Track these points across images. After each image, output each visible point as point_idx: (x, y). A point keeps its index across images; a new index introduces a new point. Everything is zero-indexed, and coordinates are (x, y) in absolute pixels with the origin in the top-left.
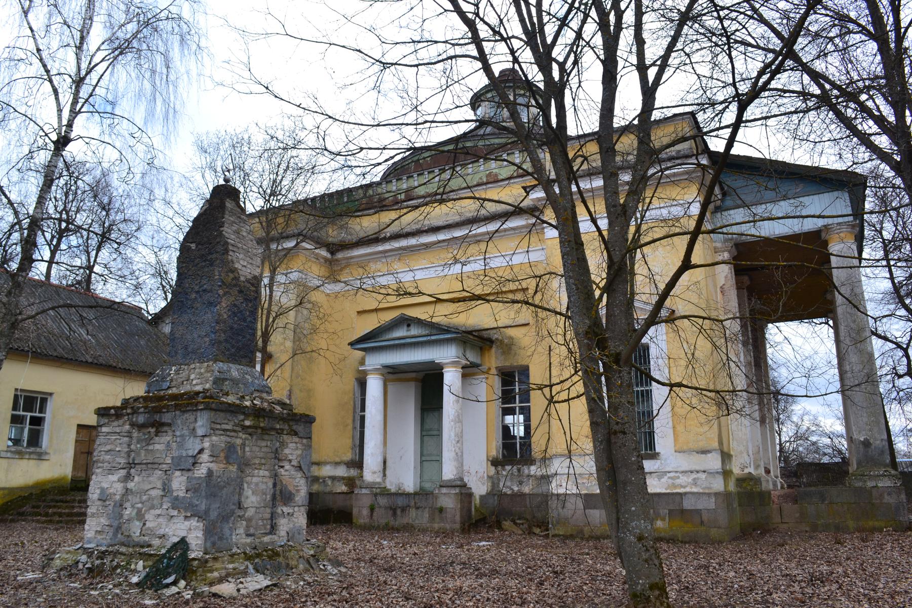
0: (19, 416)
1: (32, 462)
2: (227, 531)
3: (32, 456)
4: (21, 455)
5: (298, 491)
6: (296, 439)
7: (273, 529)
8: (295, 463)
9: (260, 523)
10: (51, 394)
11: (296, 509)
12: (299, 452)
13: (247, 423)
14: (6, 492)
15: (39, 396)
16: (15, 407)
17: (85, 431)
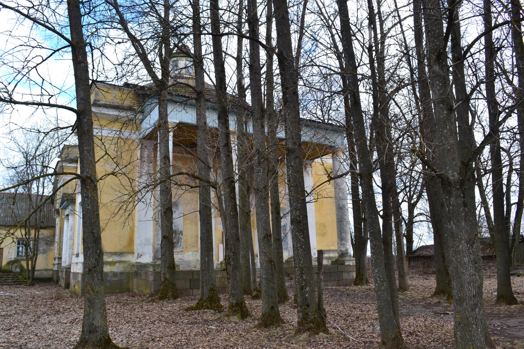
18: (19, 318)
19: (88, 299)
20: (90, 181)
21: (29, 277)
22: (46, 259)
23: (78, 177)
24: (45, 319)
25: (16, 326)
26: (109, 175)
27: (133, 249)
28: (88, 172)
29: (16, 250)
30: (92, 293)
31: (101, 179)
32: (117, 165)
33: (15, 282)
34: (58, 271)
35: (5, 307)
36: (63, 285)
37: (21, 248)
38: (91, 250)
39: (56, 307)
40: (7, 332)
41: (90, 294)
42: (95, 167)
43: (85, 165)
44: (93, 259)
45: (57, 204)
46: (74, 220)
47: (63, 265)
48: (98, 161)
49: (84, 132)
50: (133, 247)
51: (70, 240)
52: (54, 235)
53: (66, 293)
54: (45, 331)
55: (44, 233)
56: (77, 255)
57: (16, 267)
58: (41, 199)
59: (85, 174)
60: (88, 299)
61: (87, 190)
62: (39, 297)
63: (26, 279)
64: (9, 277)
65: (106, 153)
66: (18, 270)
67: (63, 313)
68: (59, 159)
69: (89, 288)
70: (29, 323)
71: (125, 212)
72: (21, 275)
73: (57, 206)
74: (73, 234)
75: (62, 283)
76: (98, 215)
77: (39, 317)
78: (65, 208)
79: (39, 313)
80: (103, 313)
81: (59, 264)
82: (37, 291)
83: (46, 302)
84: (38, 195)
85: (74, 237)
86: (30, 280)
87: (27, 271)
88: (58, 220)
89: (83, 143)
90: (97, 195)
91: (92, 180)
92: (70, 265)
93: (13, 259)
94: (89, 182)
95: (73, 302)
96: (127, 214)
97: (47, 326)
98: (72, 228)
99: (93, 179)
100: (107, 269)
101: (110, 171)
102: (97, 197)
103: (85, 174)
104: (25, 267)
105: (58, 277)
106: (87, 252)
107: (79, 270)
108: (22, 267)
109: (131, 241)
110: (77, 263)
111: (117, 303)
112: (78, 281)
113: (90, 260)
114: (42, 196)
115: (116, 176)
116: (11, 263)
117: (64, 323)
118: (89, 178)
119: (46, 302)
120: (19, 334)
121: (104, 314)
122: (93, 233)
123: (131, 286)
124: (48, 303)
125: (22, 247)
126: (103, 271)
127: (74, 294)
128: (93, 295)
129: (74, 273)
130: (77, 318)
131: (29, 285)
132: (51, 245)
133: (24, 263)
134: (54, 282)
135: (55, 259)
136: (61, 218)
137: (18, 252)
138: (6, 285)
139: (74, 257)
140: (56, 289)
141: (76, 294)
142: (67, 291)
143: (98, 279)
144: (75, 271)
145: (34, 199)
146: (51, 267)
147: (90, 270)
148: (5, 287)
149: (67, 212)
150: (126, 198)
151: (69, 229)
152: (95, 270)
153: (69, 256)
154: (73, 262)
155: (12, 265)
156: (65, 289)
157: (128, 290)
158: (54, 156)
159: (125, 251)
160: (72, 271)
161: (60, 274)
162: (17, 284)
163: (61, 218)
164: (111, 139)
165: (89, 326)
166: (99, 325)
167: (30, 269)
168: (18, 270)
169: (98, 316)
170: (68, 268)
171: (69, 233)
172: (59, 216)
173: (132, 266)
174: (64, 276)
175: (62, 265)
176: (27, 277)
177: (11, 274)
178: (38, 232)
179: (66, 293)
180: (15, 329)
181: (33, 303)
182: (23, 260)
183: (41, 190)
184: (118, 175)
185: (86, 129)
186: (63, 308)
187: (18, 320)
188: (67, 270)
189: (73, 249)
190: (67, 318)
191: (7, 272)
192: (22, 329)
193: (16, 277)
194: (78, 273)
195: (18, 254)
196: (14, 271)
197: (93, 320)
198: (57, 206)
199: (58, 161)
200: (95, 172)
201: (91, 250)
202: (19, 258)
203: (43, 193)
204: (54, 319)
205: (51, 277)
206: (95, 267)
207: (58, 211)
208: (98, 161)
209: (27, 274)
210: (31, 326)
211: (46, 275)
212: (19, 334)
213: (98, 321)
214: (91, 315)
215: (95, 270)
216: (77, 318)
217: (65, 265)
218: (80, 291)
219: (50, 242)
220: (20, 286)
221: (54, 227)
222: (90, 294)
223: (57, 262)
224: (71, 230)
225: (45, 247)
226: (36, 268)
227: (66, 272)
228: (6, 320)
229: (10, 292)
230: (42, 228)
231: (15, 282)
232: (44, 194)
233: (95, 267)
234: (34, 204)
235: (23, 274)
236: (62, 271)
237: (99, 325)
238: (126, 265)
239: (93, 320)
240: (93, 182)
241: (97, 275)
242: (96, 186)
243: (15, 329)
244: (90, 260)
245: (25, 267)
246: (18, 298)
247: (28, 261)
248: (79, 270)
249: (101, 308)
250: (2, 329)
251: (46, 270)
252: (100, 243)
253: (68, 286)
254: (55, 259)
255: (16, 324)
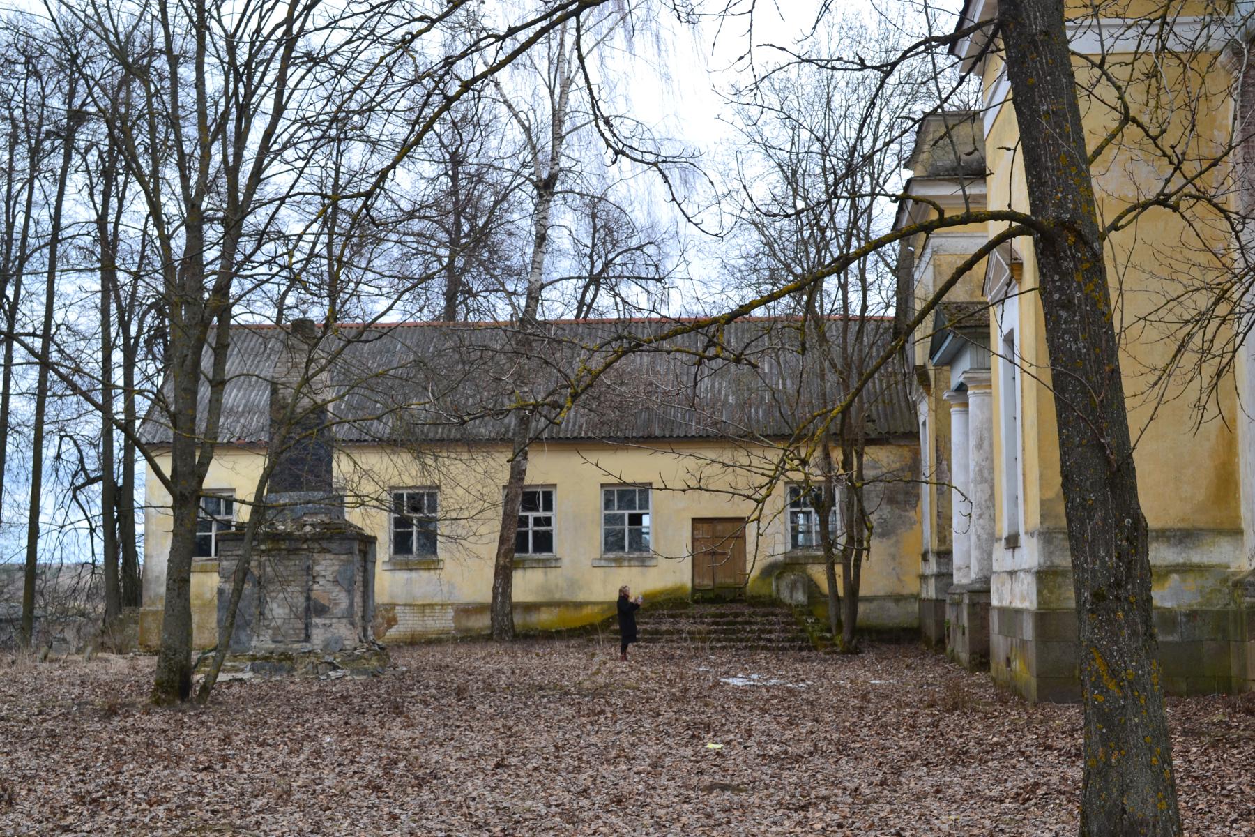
0: (615, 515)
1: (634, 570)
2: (243, 637)
3: (632, 563)
4: (618, 562)
5: (337, 604)
6: (328, 556)
7: (308, 638)
8: (331, 578)
9: (291, 632)
10: (555, 486)
11: (334, 620)
12: (336, 568)
13: (263, 547)
14: (605, 606)
15: (405, 492)
16: (608, 504)
17: (706, 526)
18: (830, 768)
19: (1099, 710)
20: (1072, 239)
21: (840, 625)
22: (893, 557)
23: (1025, 225)
24: (917, 779)
25: (825, 798)
26: (1145, 206)
27: (1238, 517)
28: (1060, 205)
29: (789, 525)
30: (1112, 686)
31: (1115, 227)
32: (1178, 168)
33: (792, 640)
34: (939, 603)
35: (774, 726)
36: (965, 656)
37: (801, 519)
38: (1099, 515)
39: (952, 736)
40: (797, 816)
41: (1104, 691)
42: (1087, 179)
43: (1046, 175)
44: (1108, 553)
45: (918, 348)
46: (990, 408)
47: (959, 578)
48: (1098, 152)
49: (1033, 42)
50: (1237, 508)
51: (977, 483)
52: (915, 465)
53: (978, 685)
54: (928, 822)
55: (880, 459)
56: (1012, 542)
57: (793, 588)
58: (860, 331)
59: (1052, 212)
60: (1099, 710)
61: (1064, 275)
62: (886, 697)
63: (829, 630)
64: (771, 623)
65: (1127, 118)
66: (800, 597)
67: (983, 762)
68: (908, 174)
69: (1098, 664)
70: (865, 789)
71: (1201, 362)
72: (810, 614)
73: (920, 354)
74: (990, 459)
75: (960, 646)
76: (1116, 373)
77: (898, 771)
78: (951, 361)
79: (894, 754)
80: (1162, 770)
81: (944, 577)
82: (873, 675)
83: (914, 716)
84: (846, 318)
85: (991, 470)
86: (845, 635)
87: (831, 602)
88: (924, 410)
89: (1032, 88)
90: (1107, 296)
91: (1079, 234)
92: (987, 580)
93: (781, 558)
94: (1065, 240)
95: (1012, 722)
96: (1209, 369)
97: (933, 805)
98: (981, 439)
99: (1086, 231)
100: (1164, 596)
101: (1152, 189)
102: (1108, 304)
103: (1052, 212)
104: (825, 587)
105: (941, 623)
106: (1083, 524)
107: (1023, 598)
108: (811, 586)
109: (1226, 483)
110: (1012, 573)
111: (1185, 733)
112: (1024, 642)
113: (1095, 556)
114: (863, 319)
115: (1175, 209)
116: (773, 570)
117: (991, 799)
118: (1069, 226)
119: (914, 716)
120: (840, 826)
121: (1167, 774)
122: (1102, 447)
123: (1234, 671)
124: (921, 720)
125: (807, 514)
126: (1149, 599)
127: (1009, 693)
128: (1118, 693)
129: (1003, 611)
130: (1037, 785)
131: (843, 653)
132: (907, 502)
133: (818, 573)
134: (928, 643)
135: (925, 557)
136: (938, 400)
137: (795, 532)
138: (764, 648)
139: (999, 550)
140: (939, 670)
141: (1015, 691)
142: (980, 677)
143: (1134, 633)
144: (1006, 603)
145: (834, 333)
146: (912, 586)
147: (1098, 596)
148: (761, 657)
149: (956, 378)
150: (1204, 301)
151: (972, 442)
152: (1118, 598)
153: (980, 547)
154: (996, 567)
155: (778, 578)
156: (972, 672)
157: (1225, 686)
158: (891, 161)
159: (1202, 525)
160: (995, 602)
161: (950, 615)
162: (801, 649)
163: (938, 400)
164: (1130, 59)
165: (1109, 815)
166: (1149, 813)
167: (841, 593)
168: (800, 597)
169: (1143, 782)
170: (980, 593)
171: (974, 458)
172: (929, 393)
173: (1236, 584)
174: (965, 621)
175: (956, 580)
176: (833, 622)
177: (778, 611)
178: (860, 456)
179: (980, 686)
180: (822, 806)
181: (868, 719)
182: (816, 560)
183: (855, 298)
184: (1183, 206)
185: (1038, 26)
186: (979, 742)
187: (826, 778)
188: (976, 599)
189: (993, 519)
190: (998, 781)
191: (764, 604)
192: (847, 812)
193: (796, 623)
194: (1018, 612)
195: (795, 544)
196: (788, 601)
197: (1122, 793)
198: (920, 354)
199: (909, 181)
200: (1090, 201)
201: (1099, 515)
202: (799, 553)
203: (865, 307)
204: (955, 782)
205: (915, 624)
206: (1118, 585)
207: (922, 373)
208: (1098, 152)
209: (832, 613)
210: (876, 800)
211: (897, 615)
212: (840, 826)
213: (1144, 801)
214: (1114, 776)
215: (1118, 598)
216: (1037, 785)
217: (965, 581)
218: (1034, 682)
219: (904, 489)
220: (813, 654)
221: (912, 436)
222: (1104, 691)
223: (932, 567)
224: (979, 446)
225: (886, 510)
226: (863, 592)
227: (973, 605)
228: (785, 774)
229: (782, 677)
230: (870, 442)
231: (792, 640)
232: (868, 314)
233: (1118, 585)
234: (836, 352)
235: (819, 611)
236: (958, 604)
237: (1149, 813)
238: (1210, 582)
239: (1122, 793)
240: (1087, 243)
241: (1126, 615)
242: (1097, 258)
243: (822, 806)
244: (1095, 556)
245: (825, 587)
246: (812, 697)
247: (833, 564)
248: (1023, 598)
249: (1150, 749)
250: (779, 803)
251: (898, 598)
252: (1133, 490)
253: (981, 659)
254: (925, 557)
255: (823, 791)
